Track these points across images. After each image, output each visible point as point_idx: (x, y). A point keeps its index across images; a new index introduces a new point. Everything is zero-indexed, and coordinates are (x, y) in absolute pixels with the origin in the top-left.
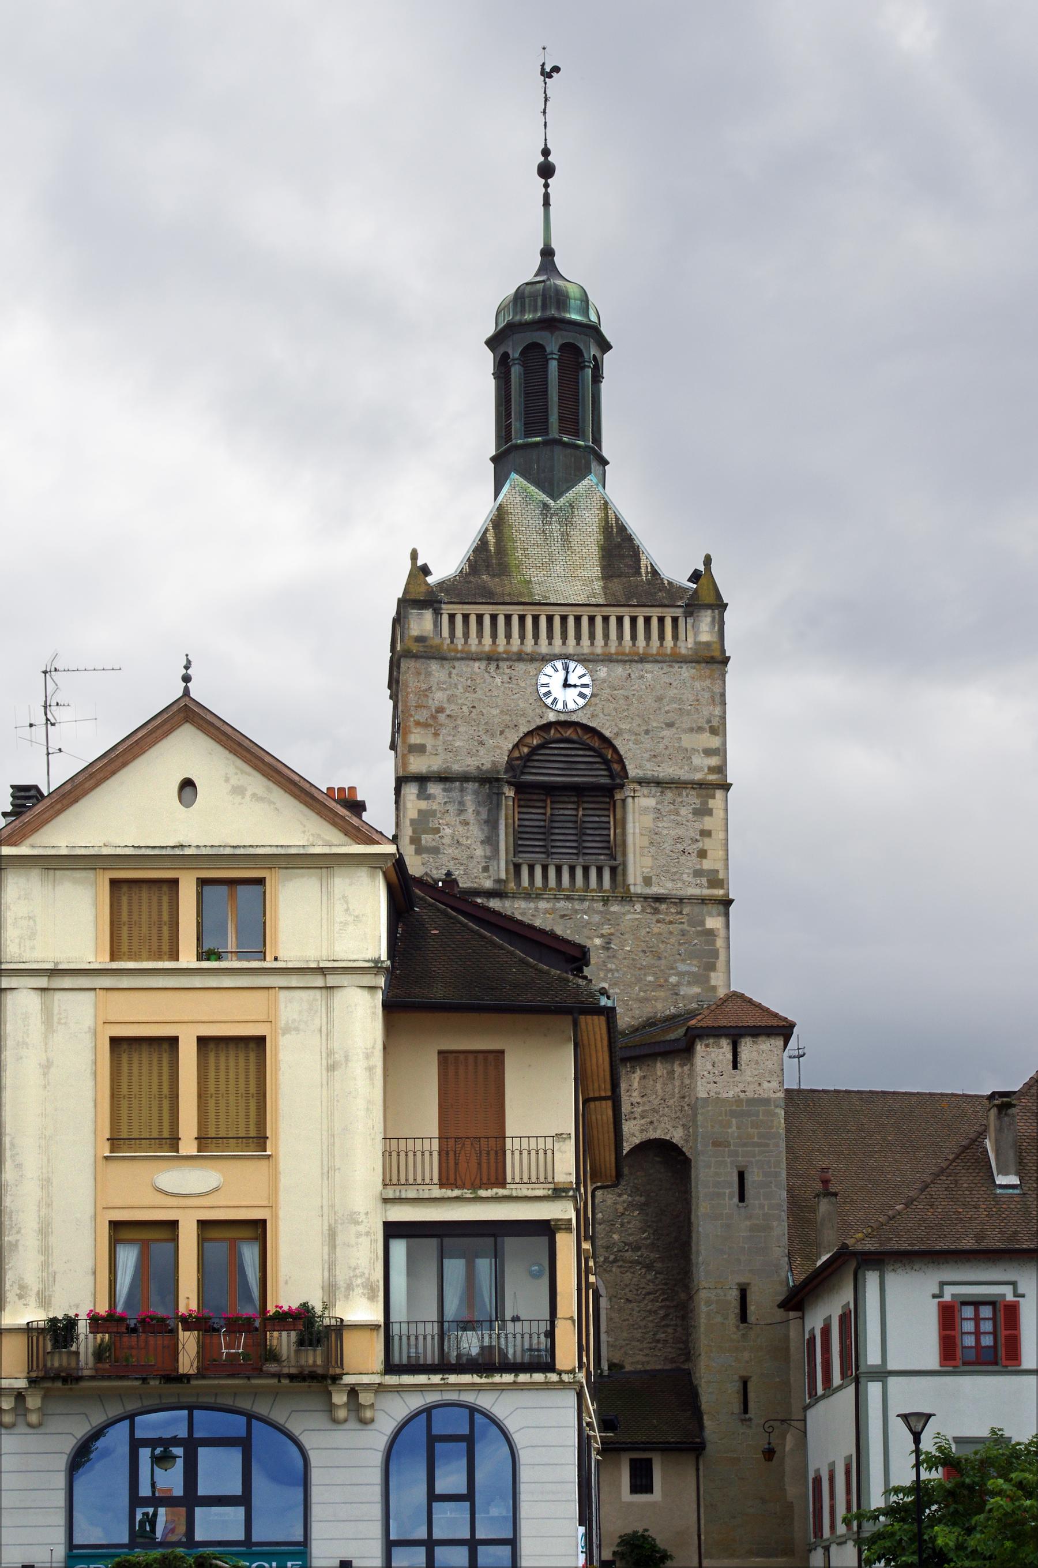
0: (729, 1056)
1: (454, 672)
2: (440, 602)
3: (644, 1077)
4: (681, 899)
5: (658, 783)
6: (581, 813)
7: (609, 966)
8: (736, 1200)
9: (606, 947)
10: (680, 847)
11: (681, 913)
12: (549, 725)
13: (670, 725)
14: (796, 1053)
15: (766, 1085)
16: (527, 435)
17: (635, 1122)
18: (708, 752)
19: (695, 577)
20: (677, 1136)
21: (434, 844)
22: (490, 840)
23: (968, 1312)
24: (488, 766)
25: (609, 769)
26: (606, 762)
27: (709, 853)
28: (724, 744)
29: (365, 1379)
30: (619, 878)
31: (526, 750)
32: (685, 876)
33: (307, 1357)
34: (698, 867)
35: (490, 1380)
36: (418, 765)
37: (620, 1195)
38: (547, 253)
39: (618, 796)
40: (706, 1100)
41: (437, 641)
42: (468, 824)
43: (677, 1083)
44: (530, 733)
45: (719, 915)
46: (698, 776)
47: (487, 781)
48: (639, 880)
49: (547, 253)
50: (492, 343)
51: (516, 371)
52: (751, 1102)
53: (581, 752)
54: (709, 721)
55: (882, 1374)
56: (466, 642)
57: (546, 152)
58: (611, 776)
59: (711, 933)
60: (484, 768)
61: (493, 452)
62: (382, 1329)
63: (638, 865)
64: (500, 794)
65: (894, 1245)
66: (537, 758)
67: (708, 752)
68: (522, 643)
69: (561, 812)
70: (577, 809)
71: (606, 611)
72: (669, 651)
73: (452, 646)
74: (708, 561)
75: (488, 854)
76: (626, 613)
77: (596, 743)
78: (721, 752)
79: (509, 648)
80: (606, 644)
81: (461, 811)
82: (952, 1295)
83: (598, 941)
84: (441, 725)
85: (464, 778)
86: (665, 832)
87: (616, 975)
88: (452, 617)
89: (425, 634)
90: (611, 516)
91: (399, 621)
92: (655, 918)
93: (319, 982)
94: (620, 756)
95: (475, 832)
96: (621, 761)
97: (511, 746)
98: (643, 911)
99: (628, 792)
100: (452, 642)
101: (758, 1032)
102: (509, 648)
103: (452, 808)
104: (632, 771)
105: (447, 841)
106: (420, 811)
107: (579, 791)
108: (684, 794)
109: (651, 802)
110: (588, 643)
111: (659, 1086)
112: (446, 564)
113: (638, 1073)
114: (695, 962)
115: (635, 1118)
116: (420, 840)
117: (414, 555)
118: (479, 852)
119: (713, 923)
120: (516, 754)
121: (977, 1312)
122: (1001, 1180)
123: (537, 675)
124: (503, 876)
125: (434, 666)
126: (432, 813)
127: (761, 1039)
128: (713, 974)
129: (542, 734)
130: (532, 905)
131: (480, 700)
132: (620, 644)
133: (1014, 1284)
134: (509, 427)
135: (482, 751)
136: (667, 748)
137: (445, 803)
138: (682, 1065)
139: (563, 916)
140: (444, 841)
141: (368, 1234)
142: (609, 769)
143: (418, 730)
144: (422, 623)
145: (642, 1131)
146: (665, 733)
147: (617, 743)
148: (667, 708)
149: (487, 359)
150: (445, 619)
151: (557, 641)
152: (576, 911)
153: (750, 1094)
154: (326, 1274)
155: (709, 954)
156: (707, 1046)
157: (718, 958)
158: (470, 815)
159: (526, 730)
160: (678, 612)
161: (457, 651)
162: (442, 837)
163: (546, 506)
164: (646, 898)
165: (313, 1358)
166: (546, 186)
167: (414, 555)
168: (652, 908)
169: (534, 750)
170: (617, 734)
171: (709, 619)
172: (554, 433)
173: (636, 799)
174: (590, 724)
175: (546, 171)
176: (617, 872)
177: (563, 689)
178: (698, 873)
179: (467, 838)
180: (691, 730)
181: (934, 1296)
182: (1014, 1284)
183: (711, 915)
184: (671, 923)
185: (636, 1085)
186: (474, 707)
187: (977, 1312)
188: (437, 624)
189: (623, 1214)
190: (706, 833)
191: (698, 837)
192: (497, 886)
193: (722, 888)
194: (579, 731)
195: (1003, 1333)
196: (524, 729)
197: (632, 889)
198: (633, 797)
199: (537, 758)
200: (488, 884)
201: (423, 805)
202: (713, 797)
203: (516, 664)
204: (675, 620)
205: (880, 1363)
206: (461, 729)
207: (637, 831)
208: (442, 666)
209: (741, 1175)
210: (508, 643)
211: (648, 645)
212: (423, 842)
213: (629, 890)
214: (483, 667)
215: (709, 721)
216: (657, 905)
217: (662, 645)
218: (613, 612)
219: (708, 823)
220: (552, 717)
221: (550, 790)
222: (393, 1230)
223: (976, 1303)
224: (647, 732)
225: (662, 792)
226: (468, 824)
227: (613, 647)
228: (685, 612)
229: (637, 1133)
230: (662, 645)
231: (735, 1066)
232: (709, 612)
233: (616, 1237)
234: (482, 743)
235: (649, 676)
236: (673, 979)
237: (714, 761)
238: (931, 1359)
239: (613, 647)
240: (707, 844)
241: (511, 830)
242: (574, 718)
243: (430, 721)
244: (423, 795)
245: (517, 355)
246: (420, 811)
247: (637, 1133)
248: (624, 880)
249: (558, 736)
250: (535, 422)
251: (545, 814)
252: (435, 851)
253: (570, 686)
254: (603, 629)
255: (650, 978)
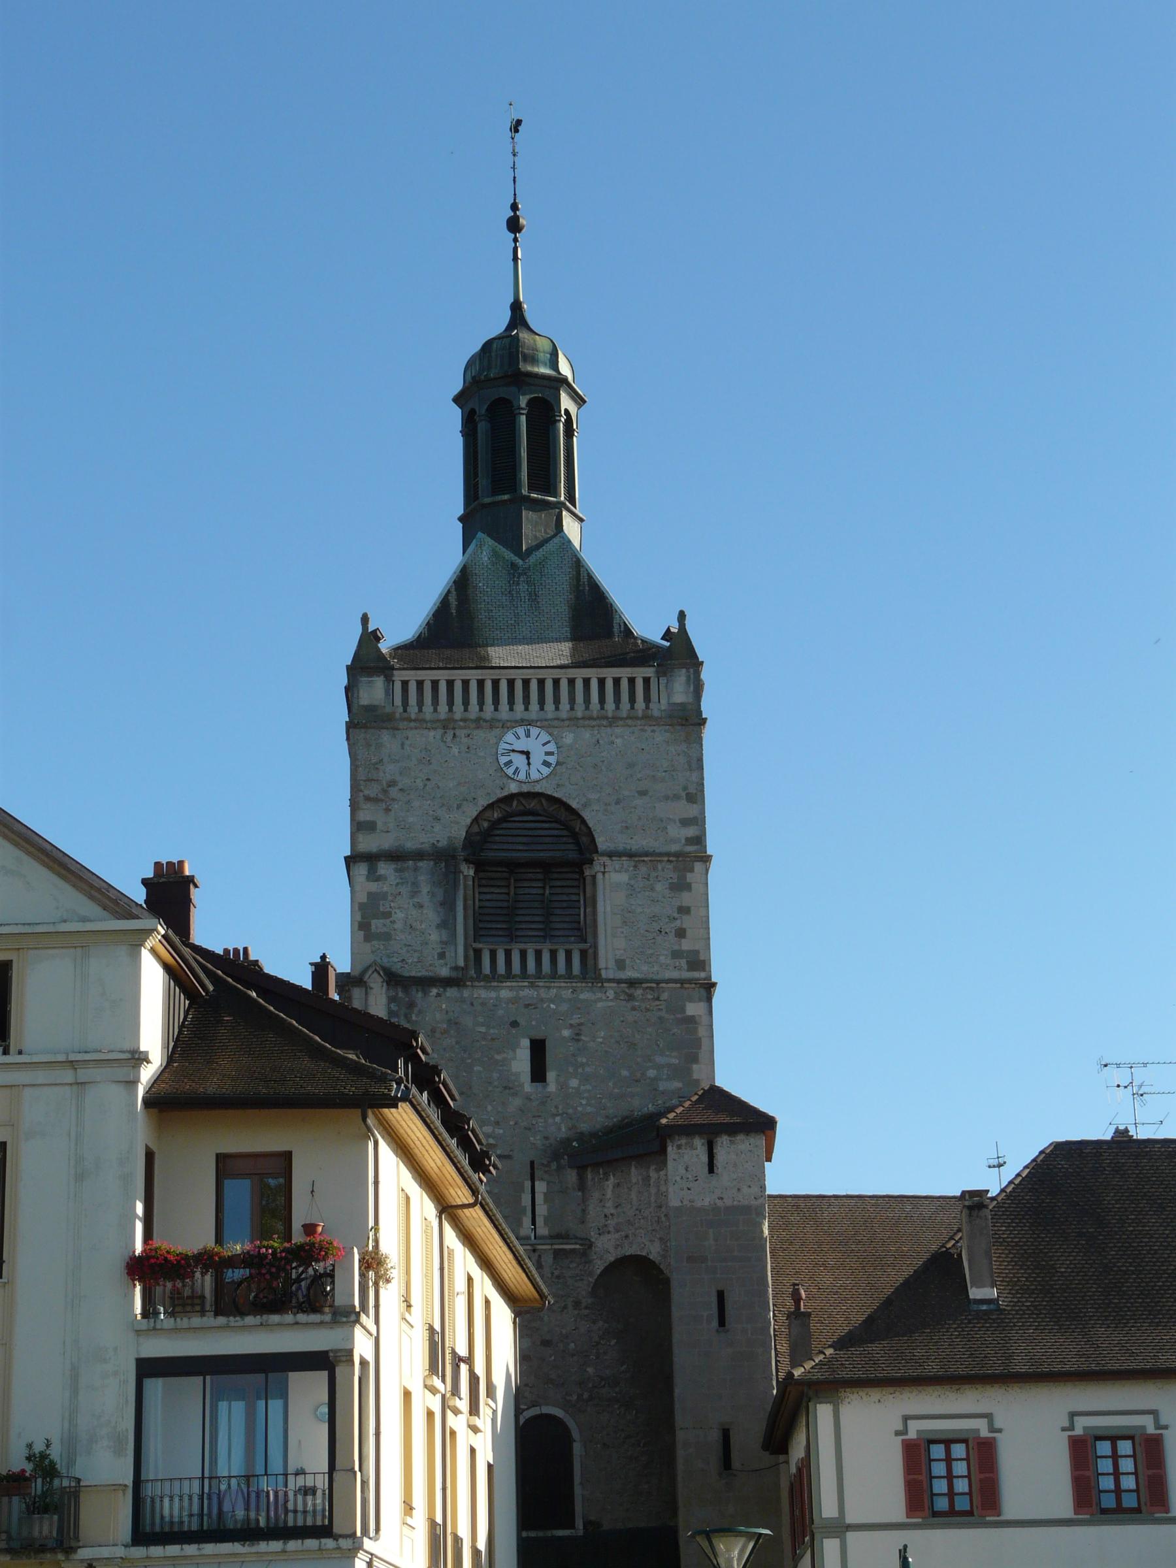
0: (704, 1158)
1: (407, 742)
2: (393, 668)
3: (618, 1185)
4: (658, 982)
5: (630, 855)
6: (547, 892)
7: (579, 1059)
8: (715, 1323)
9: (577, 1037)
10: (656, 926)
11: (658, 999)
12: (511, 797)
13: (643, 793)
14: (995, 1162)
15: (745, 1190)
16: (495, 492)
17: (609, 1236)
18: (686, 822)
19: (668, 635)
20: (654, 1251)
21: (385, 929)
22: (446, 924)
23: (1104, 1448)
24: (443, 843)
25: (577, 843)
26: (574, 835)
27: (689, 933)
28: (702, 812)
29: (105, 1552)
30: (590, 962)
31: (486, 825)
32: (662, 958)
33: (41, 1527)
34: (676, 947)
35: (254, 1549)
36: (370, 844)
37: (594, 1322)
38: (516, 307)
39: (587, 873)
40: (677, 1209)
41: (388, 710)
42: (422, 907)
43: (653, 1190)
44: (491, 806)
45: (700, 1000)
46: (674, 848)
47: (443, 857)
48: (612, 964)
49: (516, 307)
50: (458, 400)
51: (482, 427)
52: (728, 1209)
53: (546, 825)
54: (685, 788)
55: (840, 1528)
56: (420, 710)
57: (514, 207)
58: (580, 851)
59: (692, 1020)
60: (440, 845)
61: (461, 512)
62: (130, 1492)
63: (612, 945)
64: (457, 872)
65: (844, 1374)
66: (498, 832)
67: (686, 822)
68: (481, 710)
69: (527, 891)
70: (544, 888)
71: (572, 673)
72: (640, 714)
73: (405, 715)
74: (682, 616)
75: (444, 938)
76: (593, 674)
77: (563, 815)
78: (698, 821)
79: (467, 715)
80: (572, 709)
81: (415, 893)
82: (1084, 1428)
83: (566, 1033)
84: (393, 800)
85: (419, 855)
86: (639, 910)
87: (588, 1069)
88: (405, 684)
89: (376, 703)
90: (584, 574)
91: (350, 691)
92: (629, 1005)
93: (68, 1076)
94: (589, 828)
95: (431, 915)
96: (590, 834)
97: (469, 821)
98: (616, 998)
99: (597, 867)
100: (405, 711)
101: (732, 1130)
102: (467, 715)
103: (405, 890)
104: (602, 843)
105: (399, 925)
106: (370, 894)
107: (546, 867)
108: (660, 867)
109: (623, 878)
110: (522, 707)
111: (634, 1195)
112: (400, 626)
113: (612, 1180)
114: (674, 1054)
115: (609, 1232)
116: (369, 924)
117: (365, 619)
118: (434, 936)
119: (692, 1009)
120: (476, 829)
121: (948, 1451)
122: (975, 1293)
123: (497, 744)
124: (461, 963)
125: (385, 737)
126: (384, 896)
127: (740, 1137)
128: (695, 1067)
129: (503, 806)
130: (493, 994)
131: (435, 771)
132: (587, 708)
133: (989, 1417)
134: (476, 485)
135: (438, 828)
136: (640, 819)
137: (397, 884)
138: (658, 1170)
139: (527, 1006)
140: (396, 926)
141: (116, 1374)
142: (577, 843)
143: (369, 805)
144: (374, 691)
145: (617, 1246)
146: (639, 802)
147: (586, 815)
148: (639, 776)
149: (455, 415)
150: (398, 687)
151: (519, 706)
152: (542, 1000)
153: (728, 1202)
154: (66, 1425)
155: (694, 1042)
156: (679, 1147)
157: (699, 1047)
158: (424, 897)
159: (486, 803)
160: (649, 672)
161: (410, 720)
162: (393, 922)
163: (513, 565)
164: (619, 981)
165: (46, 1527)
166: (515, 240)
167: (365, 619)
168: (626, 994)
169: (495, 824)
170: (585, 806)
171: (683, 679)
172: (525, 492)
173: (607, 875)
174: (556, 795)
175: (514, 225)
176: (589, 957)
177: (530, 756)
178: (676, 954)
179: (421, 922)
180: (667, 798)
181: (898, 1433)
182: (989, 1417)
183: (691, 1000)
184: (647, 1010)
185: (609, 1194)
186: (428, 779)
187: (948, 1451)
188: (389, 692)
189: (598, 1343)
190: (684, 910)
191: (676, 915)
192: (454, 974)
193: (704, 970)
194: (543, 801)
195: (923, 1477)
196: (483, 802)
197: (603, 973)
198: (604, 873)
199: (498, 832)
200: (445, 972)
201: (374, 887)
202: (692, 870)
203: (475, 732)
204: (647, 681)
205: (837, 1515)
206: (416, 804)
207: (608, 909)
208: (394, 736)
209: (721, 1295)
210: (466, 710)
211: (618, 708)
212: (373, 927)
213: (600, 975)
214: (439, 737)
215: (685, 788)
216: (632, 991)
217: (632, 708)
218: (579, 674)
219: (686, 899)
220: (513, 788)
221: (513, 866)
222: (148, 1368)
223: (1114, 1439)
224: (618, 802)
225: (635, 866)
226: (422, 907)
227: (580, 711)
228: (657, 672)
229: (612, 1250)
230: (632, 708)
231: (711, 1169)
232: (684, 671)
233: (590, 1370)
234: (437, 819)
235: (619, 741)
236: (651, 1073)
237: (691, 832)
238: (1062, 1502)
239: (580, 711)
240: (686, 922)
241: (470, 912)
242: (538, 789)
243: (381, 796)
244: (373, 876)
245: (483, 412)
246: (370, 894)
247: (612, 1250)
248: (596, 964)
249: (521, 808)
250: (504, 478)
251: (508, 894)
252: (386, 937)
253: (522, 752)
254: (569, 692)
255: (625, 1073)
